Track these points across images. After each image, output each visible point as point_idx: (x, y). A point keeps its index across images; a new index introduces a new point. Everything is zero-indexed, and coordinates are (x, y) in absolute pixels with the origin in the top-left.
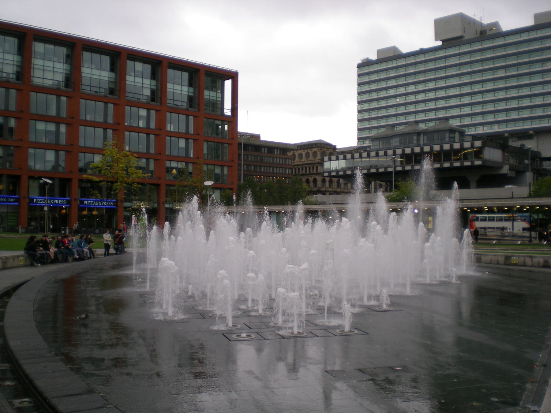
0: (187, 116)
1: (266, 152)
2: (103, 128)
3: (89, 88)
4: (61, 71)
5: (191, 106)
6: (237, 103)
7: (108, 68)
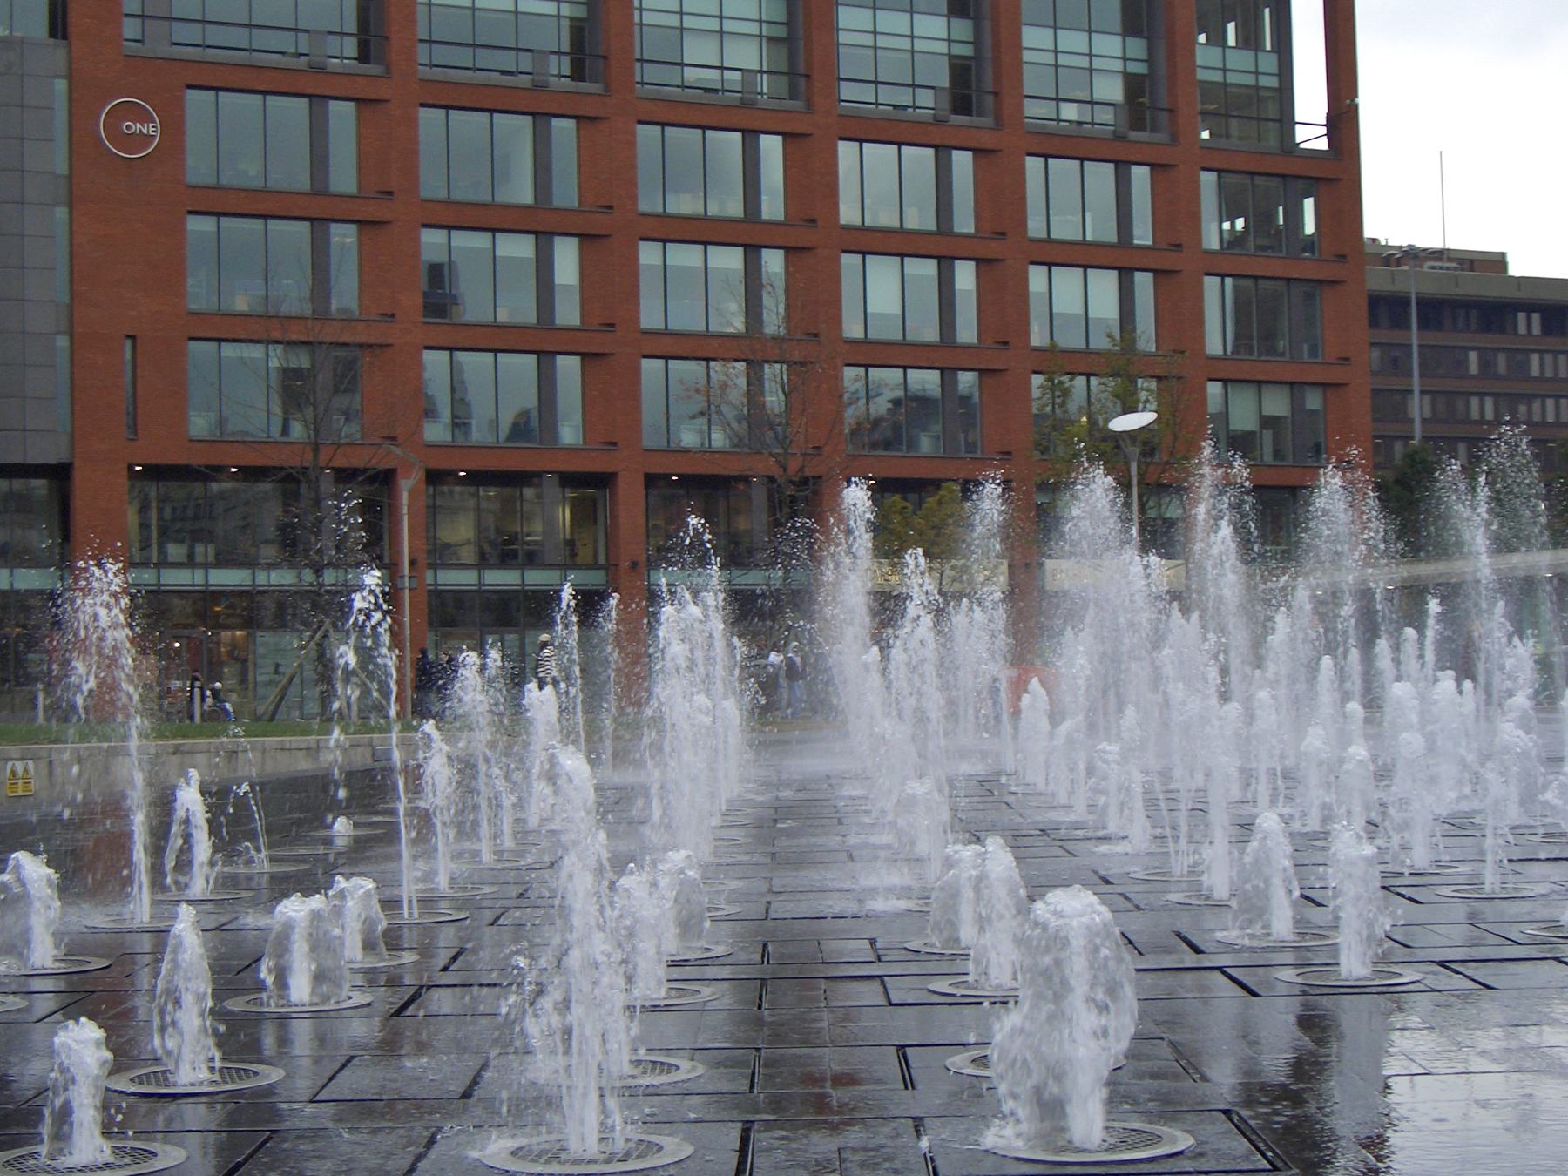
0: (1122, 168)
1: (1536, 330)
2: (939, 258)
3: (464, 57)
4: (753, 28)
5: (1137, 122)
6: (1354, 92)
7: (1117, 25)
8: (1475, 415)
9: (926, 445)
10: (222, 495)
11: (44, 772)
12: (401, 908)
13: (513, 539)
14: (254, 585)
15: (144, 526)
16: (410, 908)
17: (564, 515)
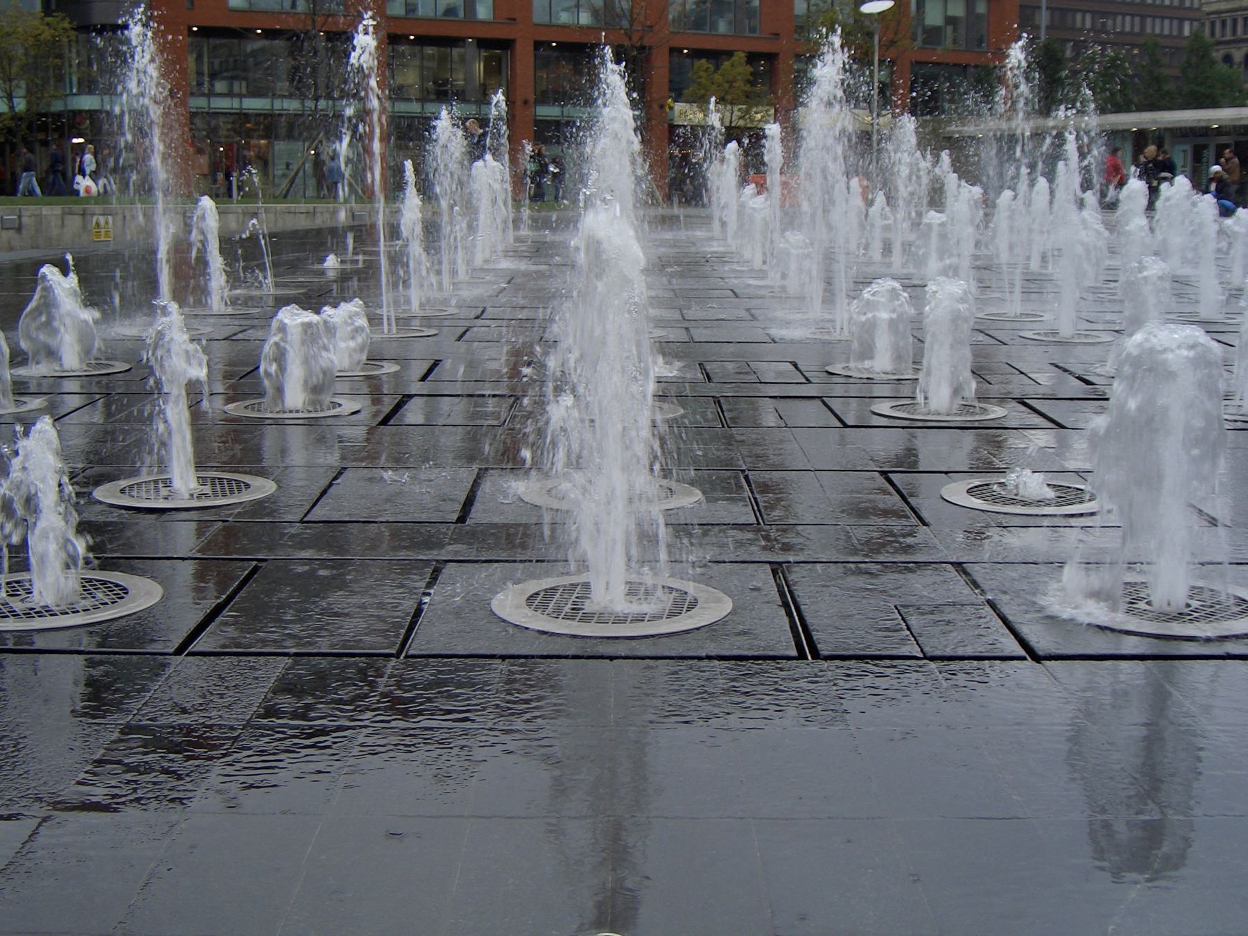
8: (1079, 24)
9: (722, 27)
10: (254, 54)
11: (120, 224)
12: (382, 324)
13: (446, 82)
14: (272, 109)
15: (200, 73)
16: (389, 324)
17: (479, 68)
